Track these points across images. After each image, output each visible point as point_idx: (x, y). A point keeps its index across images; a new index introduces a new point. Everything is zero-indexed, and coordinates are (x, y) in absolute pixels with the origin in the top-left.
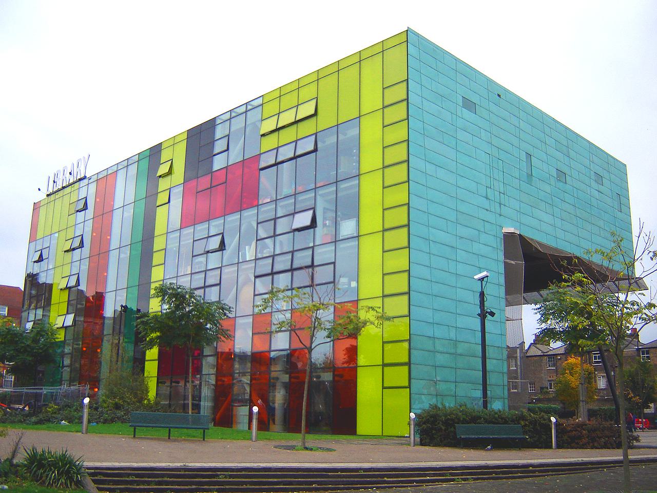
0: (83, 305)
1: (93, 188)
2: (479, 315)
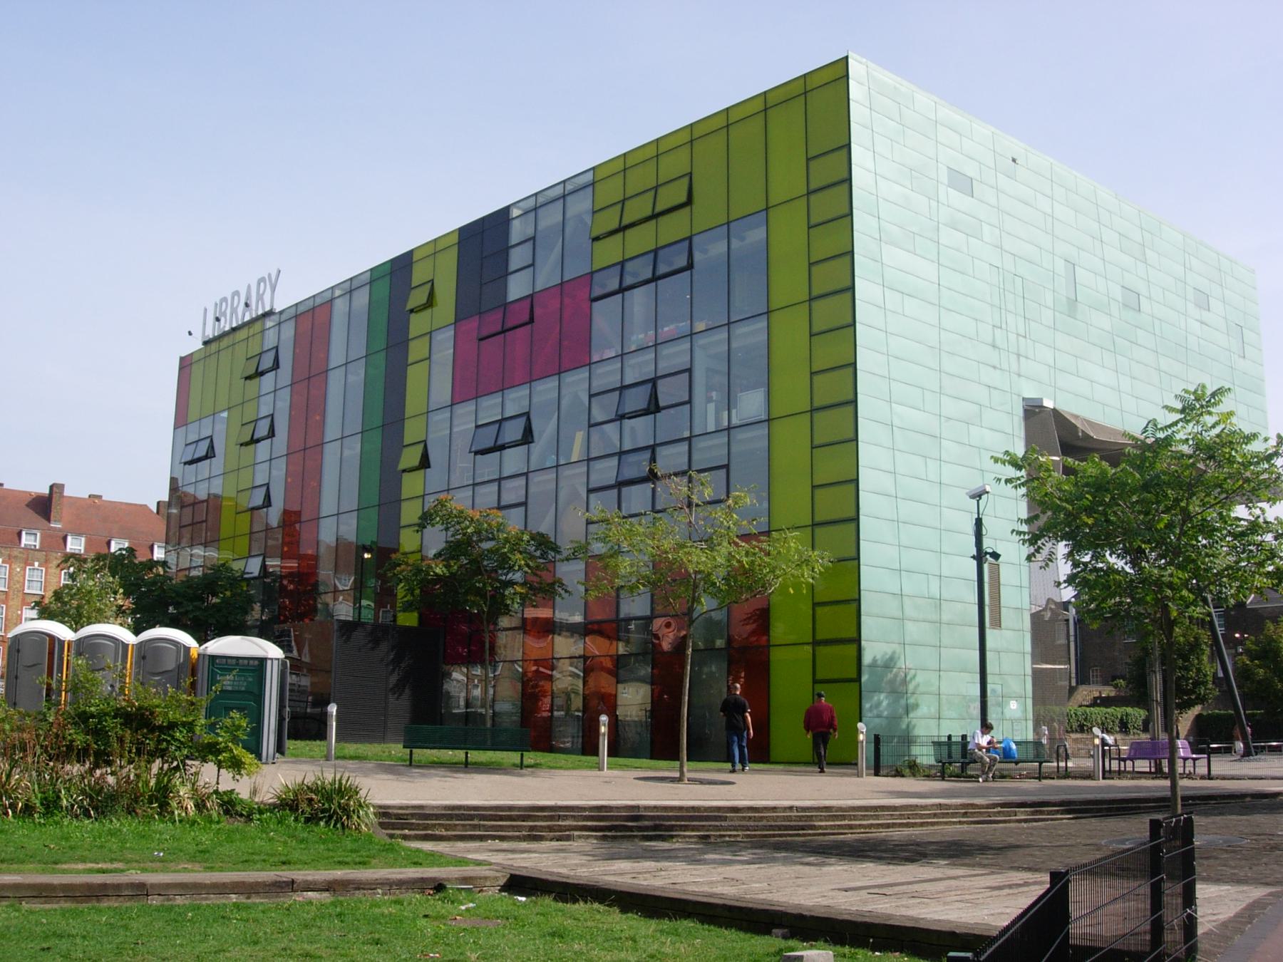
0: (277, 539)
1: (288, 331)
2: (973, 557)
